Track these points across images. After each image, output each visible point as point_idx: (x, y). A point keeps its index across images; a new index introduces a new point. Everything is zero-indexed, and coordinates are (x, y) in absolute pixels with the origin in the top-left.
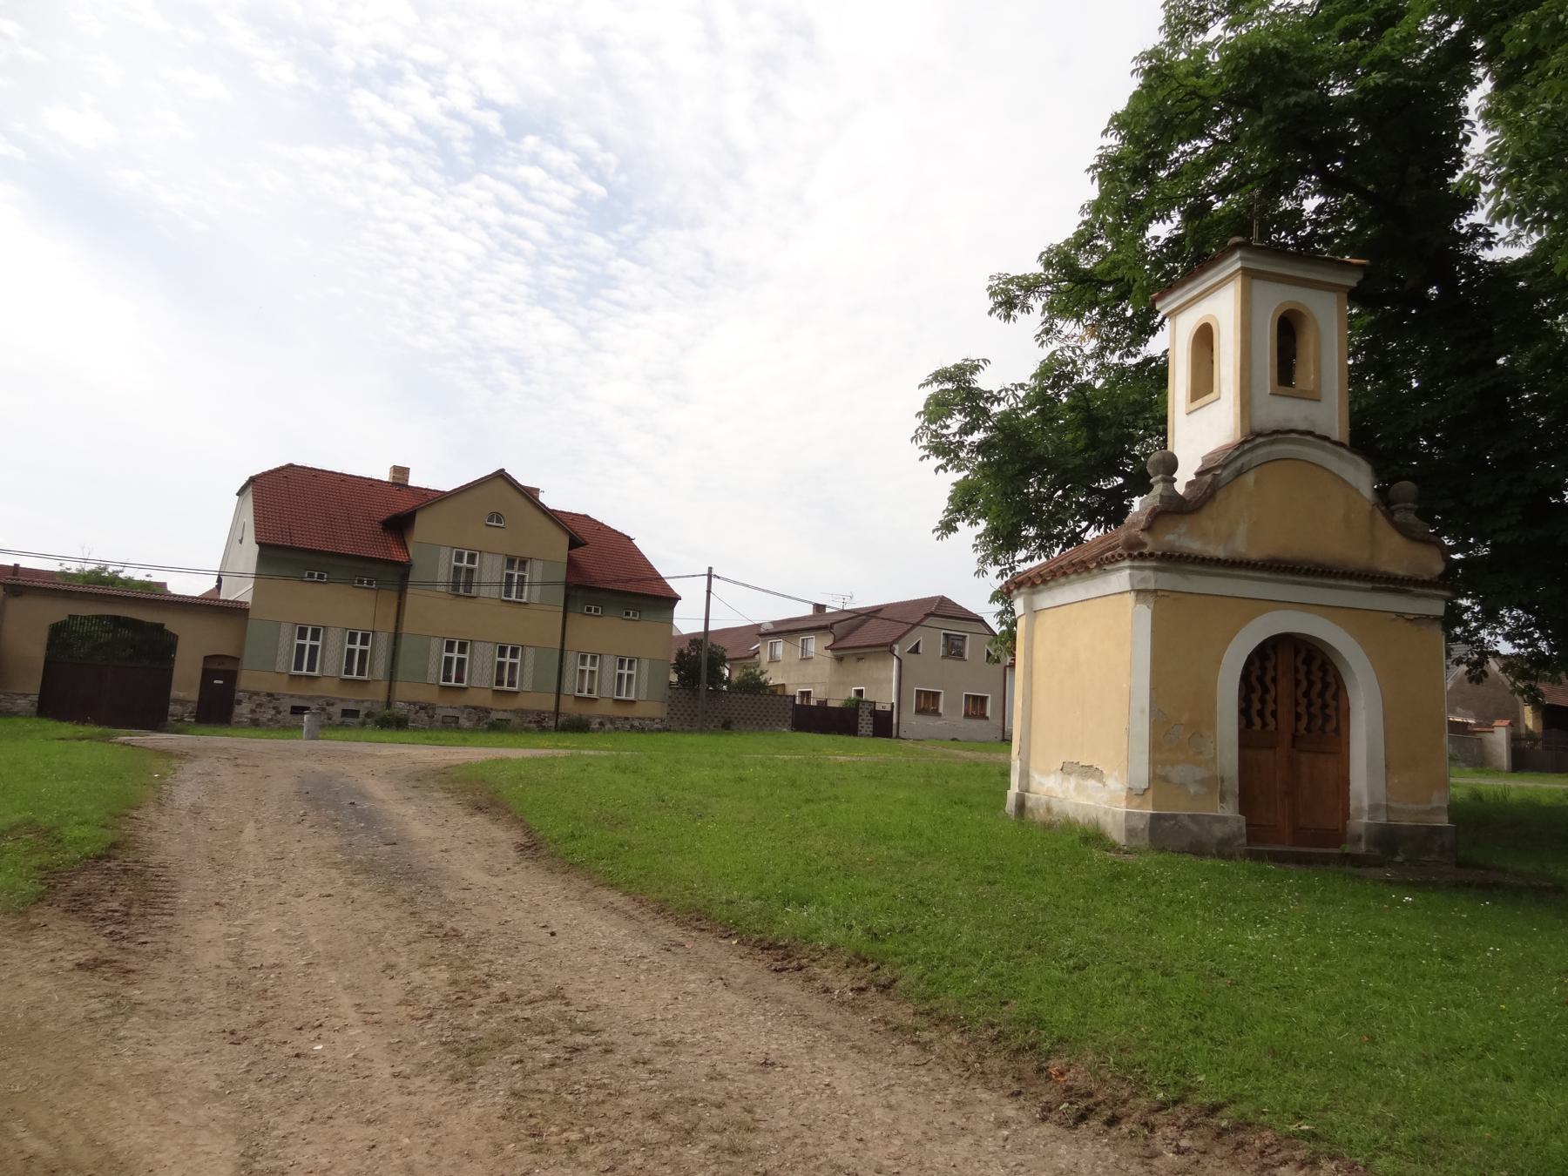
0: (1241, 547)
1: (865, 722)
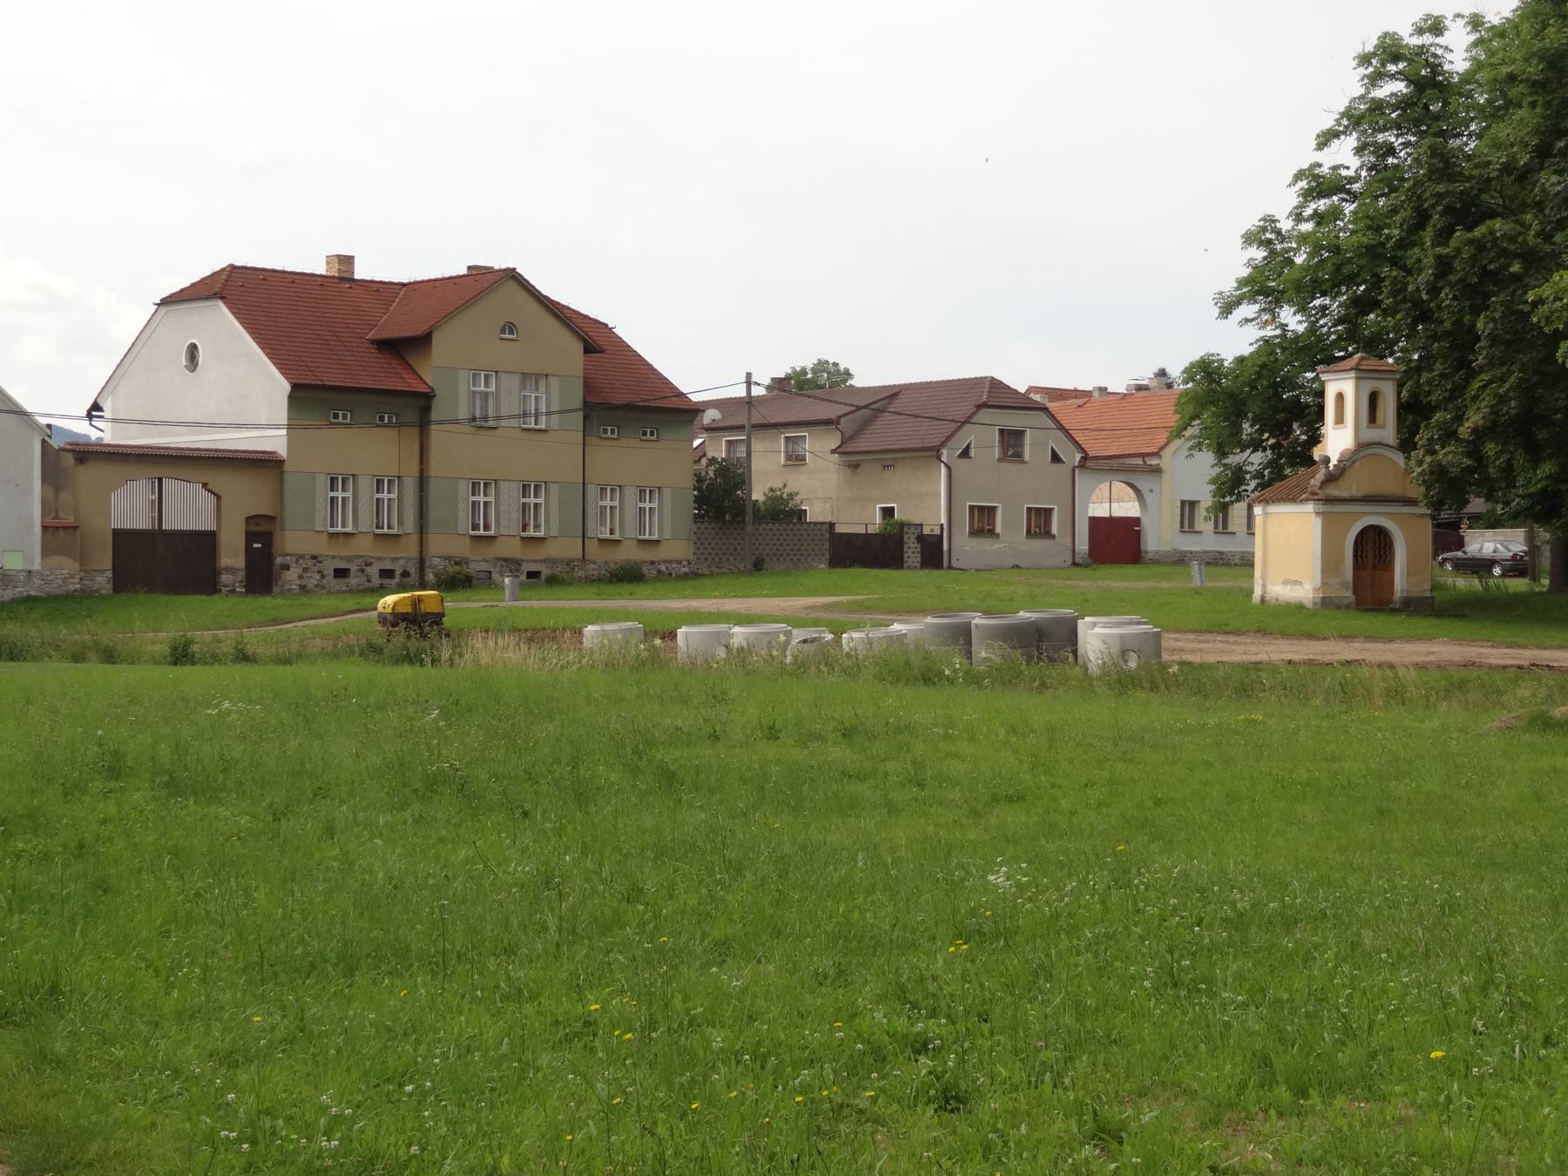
0: (1355, 491)
1: (912, 552)
